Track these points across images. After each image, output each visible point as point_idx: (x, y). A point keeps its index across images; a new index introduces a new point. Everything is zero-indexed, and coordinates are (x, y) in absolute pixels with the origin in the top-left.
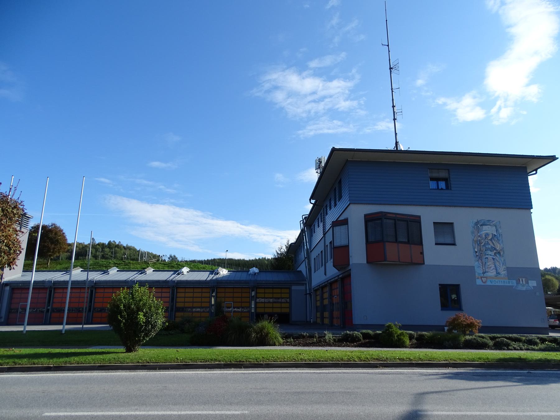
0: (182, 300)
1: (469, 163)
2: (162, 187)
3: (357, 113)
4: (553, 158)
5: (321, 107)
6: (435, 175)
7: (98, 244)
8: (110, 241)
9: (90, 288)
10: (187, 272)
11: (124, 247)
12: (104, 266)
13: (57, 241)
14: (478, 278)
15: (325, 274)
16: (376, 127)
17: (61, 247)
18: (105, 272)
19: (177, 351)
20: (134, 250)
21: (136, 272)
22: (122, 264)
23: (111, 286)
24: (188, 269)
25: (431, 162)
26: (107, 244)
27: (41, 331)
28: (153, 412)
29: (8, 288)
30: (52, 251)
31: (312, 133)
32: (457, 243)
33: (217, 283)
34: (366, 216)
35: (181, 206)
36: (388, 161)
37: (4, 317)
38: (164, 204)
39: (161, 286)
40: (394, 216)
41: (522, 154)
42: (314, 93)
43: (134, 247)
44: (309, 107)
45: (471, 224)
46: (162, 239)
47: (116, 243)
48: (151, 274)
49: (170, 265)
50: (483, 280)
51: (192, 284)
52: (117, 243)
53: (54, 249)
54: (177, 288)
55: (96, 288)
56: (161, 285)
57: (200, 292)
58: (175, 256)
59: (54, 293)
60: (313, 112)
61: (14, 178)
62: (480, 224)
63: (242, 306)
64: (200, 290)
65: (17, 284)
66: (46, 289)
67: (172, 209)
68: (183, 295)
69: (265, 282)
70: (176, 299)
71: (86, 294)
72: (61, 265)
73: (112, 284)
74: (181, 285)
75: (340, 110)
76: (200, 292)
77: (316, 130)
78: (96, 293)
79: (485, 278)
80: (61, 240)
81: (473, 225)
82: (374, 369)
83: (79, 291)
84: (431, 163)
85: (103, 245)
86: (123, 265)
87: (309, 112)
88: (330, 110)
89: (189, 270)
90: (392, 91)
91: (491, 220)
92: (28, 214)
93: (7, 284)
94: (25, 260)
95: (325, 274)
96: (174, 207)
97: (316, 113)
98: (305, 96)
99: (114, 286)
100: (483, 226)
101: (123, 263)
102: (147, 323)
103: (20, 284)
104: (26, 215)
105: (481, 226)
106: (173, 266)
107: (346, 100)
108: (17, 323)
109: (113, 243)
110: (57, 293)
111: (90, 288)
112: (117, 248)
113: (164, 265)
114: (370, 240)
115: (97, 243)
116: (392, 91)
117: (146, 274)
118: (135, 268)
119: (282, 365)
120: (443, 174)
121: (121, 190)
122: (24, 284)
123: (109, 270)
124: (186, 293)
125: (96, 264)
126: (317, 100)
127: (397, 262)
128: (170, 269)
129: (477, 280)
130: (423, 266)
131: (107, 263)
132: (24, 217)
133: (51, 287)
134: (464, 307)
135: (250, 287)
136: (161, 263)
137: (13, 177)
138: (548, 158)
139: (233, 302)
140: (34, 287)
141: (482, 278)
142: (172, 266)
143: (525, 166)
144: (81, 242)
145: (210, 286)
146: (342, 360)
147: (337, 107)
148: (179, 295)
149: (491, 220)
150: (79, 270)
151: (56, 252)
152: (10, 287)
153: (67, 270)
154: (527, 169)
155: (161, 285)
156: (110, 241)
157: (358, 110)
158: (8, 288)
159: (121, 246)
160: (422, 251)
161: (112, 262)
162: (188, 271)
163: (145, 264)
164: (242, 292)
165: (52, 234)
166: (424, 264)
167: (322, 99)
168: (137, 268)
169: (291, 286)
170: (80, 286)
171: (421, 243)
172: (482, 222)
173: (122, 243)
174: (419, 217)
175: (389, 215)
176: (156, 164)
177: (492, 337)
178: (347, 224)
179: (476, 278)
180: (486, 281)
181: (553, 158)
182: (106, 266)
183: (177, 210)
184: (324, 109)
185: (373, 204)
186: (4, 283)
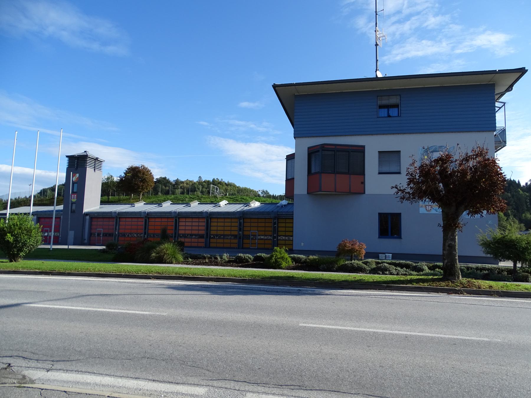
0: (283, 229)
1: (424, 86)
2: (252, 126)
3: (450, 28)
4: (522, 71)
5: (406, 27)
6: (385, 102)
7: (205, 182)
8: (214, 178)
9: (274, 218)
10: (226, 205)
11: (225, 183)
12: (181, 200)
13: (145, 179)
14: (422, 207)
16: (474, 43)
17: (148, 184)
18: (188, 204)
19: (43, 262)
20: (234, 186)
21: (242, 205)
22: (196, 198)
23: (160, 217)
24: (227, 201)
25: (382, 89)
26: (211, 181)
27: (82, 249)
28: (336, 327)
29: (88, 217)
30: (141, 188)
31: (398, 58)
33: (243, 214)
34: (309, 148)
35: (272, 143)
36: (335, 92)
37: (87, 239)
38: (256, 142)
39: (198, 217)
40: (334, 147)
41: (473, 71)
42: (399, 12)
43: (234, 184)
44: (393, 29)
45: (421, 151)
46: (259, 175)
47: (219, 180)
48: (224, 206)
49: (235, 199)
50: (428, 208)
52: (220, 180)
53: (142, 186)
54: (211, 218)
55: (149, 218)
56: (198, 216)
57: (230, 222)
58: (267, 191)
59: (120, 221)
60: (398, 33)
61: (17, 133)
62: (431, 151)
63: (266, 234)
64: (256, 221)
65: (94, 214)
66: (113, 218)
67: (265, 147)
68: (283, 225)
69: (285, 213)
70: (210, 228)
71: (142, 223)
72: (150, 199)
73: (160, 215)
74: (247, 216)
75: (429, 28)
76: (230, 222)
77: (402, 54)
78: (149, 221)
79: (429, 207)
80: (147, 179)
81: (422, 152)
82: (149, 280)
83: (137, 220)
84: (381, 90)
85: (208, 183)
86: (197, 199)
87: (394, 34)
88: (417, 30)
89: (228, 203)
91: (444, 146)
92: (99, 158)
93: (87, 214)
94: (101, 196)
96: (266, 144)
97: (402, 35)
98: (389, 16)
99: (162, 217)
100: (434, 153)
101: (197, 197)
102: (16, 241)
104: (98, 159)
105: (432, 153)
106: (237, 200)
107: (436, 15)
108: (96, 244)
109: (217, 180)
110: (151, 221)
111: (274, 218)
112: (219, 184)
113: (230, 199)
114: (313, 171)
115: (203, 181)
117: (190, 206)
118: (205, 202)
119: (80, 274)
120: (394, 100)
121: (218, 131)
122: (98, 214)
123: (162, 204)
124: (259, 223)
125: (176, 198)
126: (402, 20)
127: (333, 192)
128: (234, 203)
129: (421, 209)
130: (364, 195)
131: (184, 198)
132: (97, 161)
133: (176, 217)
134: (403, 236)
135: (272, 217)
136: (227, 197)
137: (17, 132)
138: (511, 71)
139: (258, 231)
140: (56, 216)
141: (427, 207)
142: (237, 200)
143: (492, 83)
144: (191, 180)
145: (238, 217)
146: (224, 276)
147: (425, 24)
148: (246, 224)
149: (444, 146)
150: (142, 203)
151: (145, 188)
152: (37, 217)
153: (215, 203)
154: (495, 86)
155: (198, 216)
156: (214, 178)
157: (451, 26)
158: (88, 217)
159: (224, 183)
160: (363, 181)
161: (188, 197)
162: (226, 203)
163: (214, 198)
165: (140, 174)
166: (364, 193)
167: (408, 17)
168: (207, 202)
170: (137, 216)
171: (363, 173)
172: (433, 149)
173: (223, 180)
174: (363, 147)
175: (326, 146)
176: (245, 104)
177: (51, 249)
179: (420, 207)
180: (430, 209)
181: (522, 71)
182: (183, 200)
183: (269, 147)
184: (410, 29)
185: (317, 137)
186: (85, 213)
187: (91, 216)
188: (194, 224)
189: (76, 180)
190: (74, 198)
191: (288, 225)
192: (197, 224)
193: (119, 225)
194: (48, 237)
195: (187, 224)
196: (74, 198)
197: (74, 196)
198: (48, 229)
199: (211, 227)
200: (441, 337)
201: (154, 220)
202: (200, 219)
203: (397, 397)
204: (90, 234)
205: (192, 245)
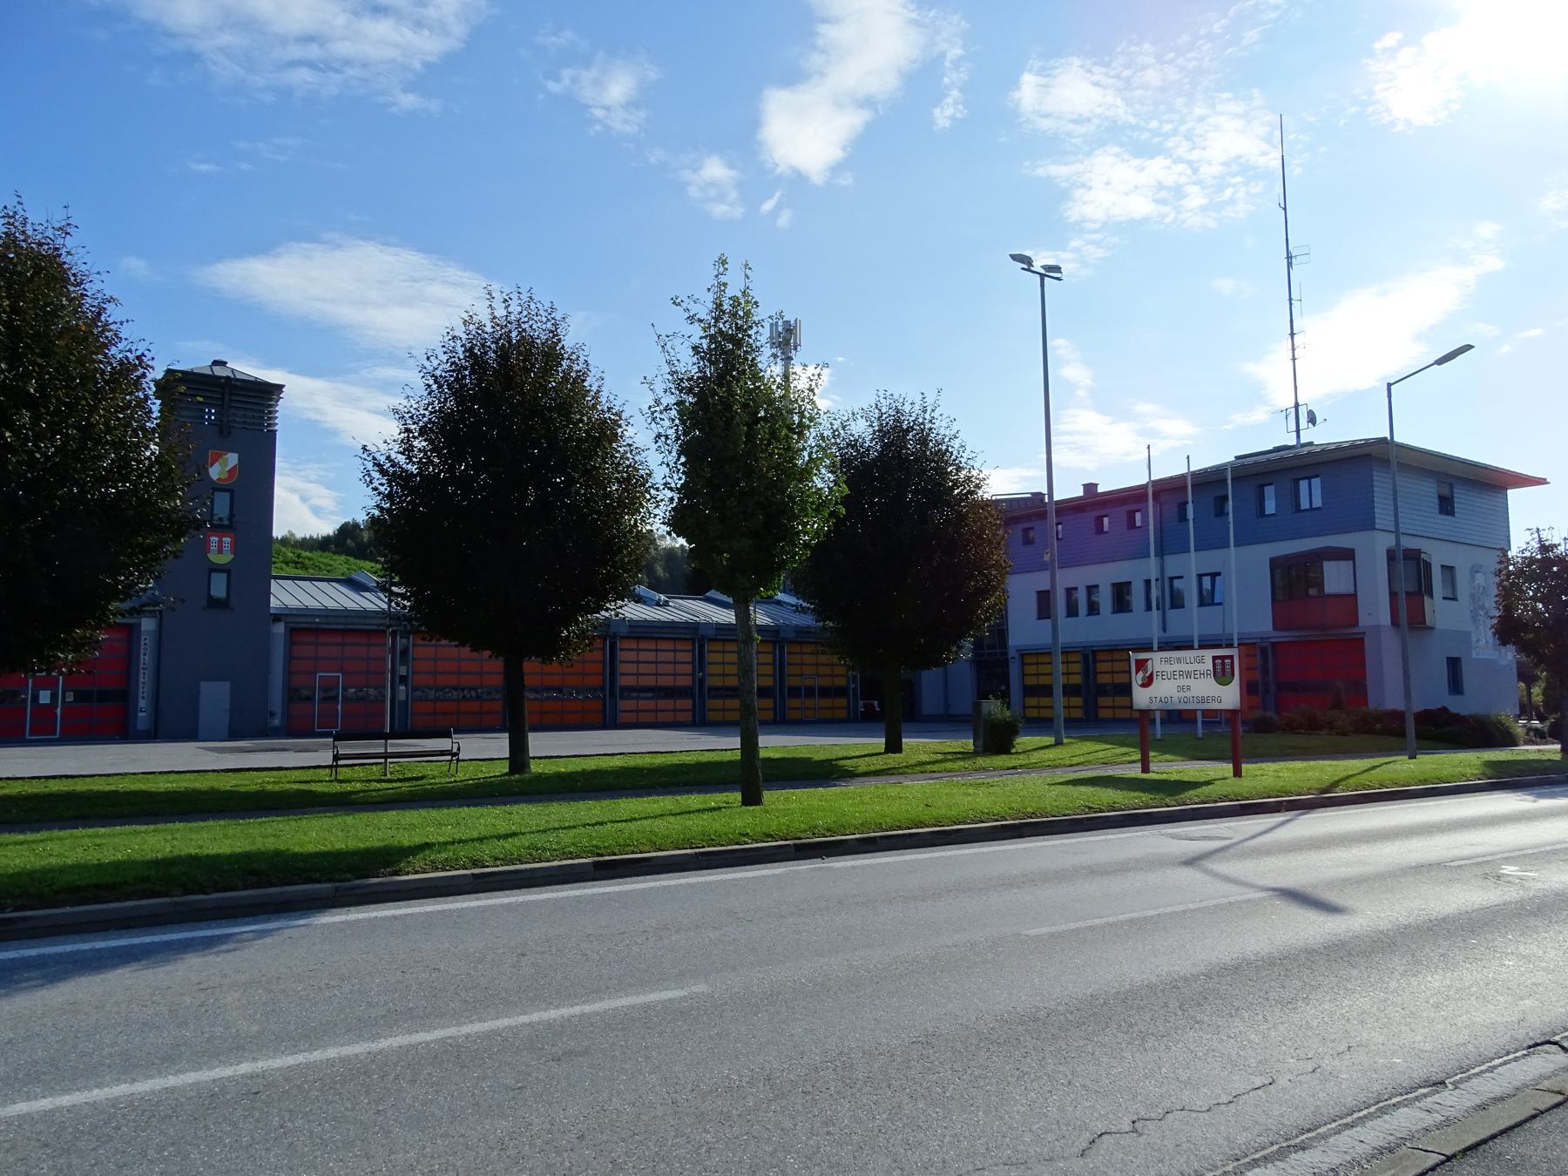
4: (1542, 482)
15: (1164, 630)
32: (1459, 598)
33: (797, 632)
51: (362, 621)
68: (632, 656)
83: (339, 639)
90: (1291, 304)
95: (1164, 630)
103: (317, 616)
116: (1291, 304)
152: (285, 627)
164: (674, 651)
169: (140, 618)
178: (1353, 559)
187: (291, 625)
188: (662, 656)
189: (225, 476)
190: (220, 551)
191: (1043, 669)
192: (669, 656)
193: (603, 662)
194: (59, 711)
195: (643, 656)
196: (220, 551)
197: (220, 543)
198: (318, 675)
199: (771, 672)
200: (1089, 866)
201: (635, 646)
202: (677, 642)
203: (199, 1175)
204: (293, 695)
205: (1117, 716)
